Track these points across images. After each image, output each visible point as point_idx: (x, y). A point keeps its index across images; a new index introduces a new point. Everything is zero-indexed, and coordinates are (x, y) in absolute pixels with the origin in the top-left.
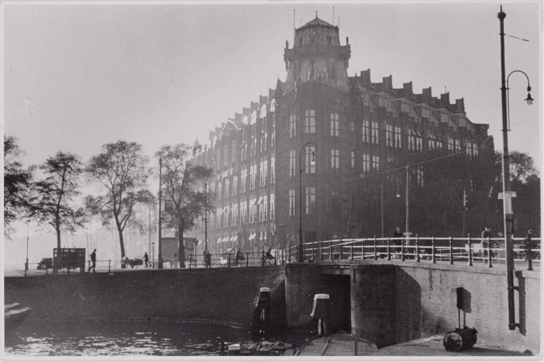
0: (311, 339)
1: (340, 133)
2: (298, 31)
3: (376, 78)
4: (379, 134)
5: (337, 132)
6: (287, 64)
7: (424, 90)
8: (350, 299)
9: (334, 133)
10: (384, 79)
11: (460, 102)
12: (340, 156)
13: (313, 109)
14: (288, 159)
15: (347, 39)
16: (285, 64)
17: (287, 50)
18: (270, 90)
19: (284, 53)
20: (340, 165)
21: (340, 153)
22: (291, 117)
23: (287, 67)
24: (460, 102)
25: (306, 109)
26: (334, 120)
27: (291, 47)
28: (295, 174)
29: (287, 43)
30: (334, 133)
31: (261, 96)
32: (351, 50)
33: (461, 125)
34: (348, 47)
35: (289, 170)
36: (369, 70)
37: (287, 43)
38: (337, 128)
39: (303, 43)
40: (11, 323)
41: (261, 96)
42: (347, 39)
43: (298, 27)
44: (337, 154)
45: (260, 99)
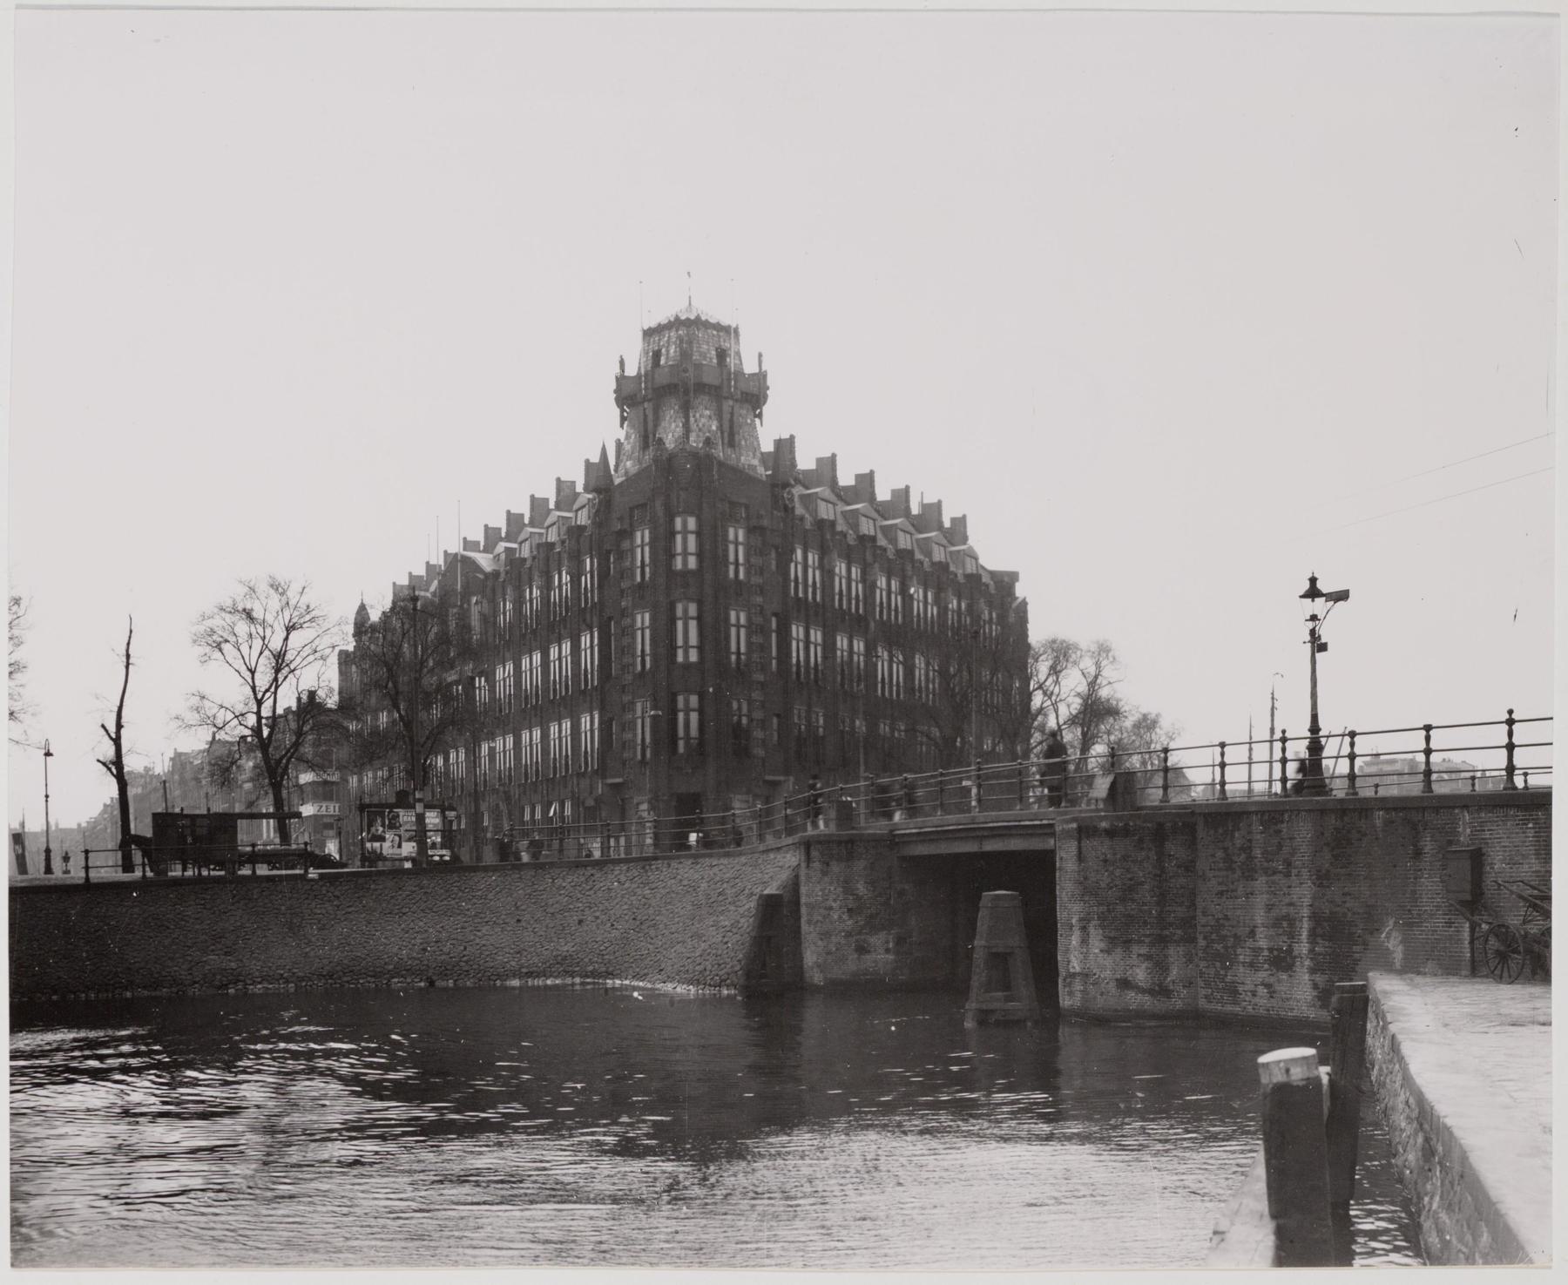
0: (1306, 1087)
1: (748, 573)
2: (648, 333)
3: (805, 461)
4: (823, 582)
5: (741, 569)
6: (623, 411)
7: (819, 461)
8: (71, 1025)
9: (737, 572)
10: (819, 461)
11: (960, 522)
12: (750, 626)
13: (691, 514)
14: (629, 631)
15: (760, 355)
16: (618, 411)
17: (621, 380)
18: (588, 463)
19: (614, 386)
20: (749, 644)
21: (749, 619)
22: (639, 534)
23: (623, 419)
24: (960, 522)
25: (679, 514)
26: (736, 543)
27: (375, 616)
28: (648, 666)
29: (622, 363)
30: (737, 572)
31: (532, 497)
32: (769, 383)
33: (969, 571)
34: (761, 377)
35: (634, 655)
36: (792, 437)
37: (622, 363)
38: (741, 560)
39: (662, 362)
40: (1413, 1241)
41: (532, 497)
42: (760, 355)
43: (652, 323)
44: (743, 621)
45: (508, 520)
